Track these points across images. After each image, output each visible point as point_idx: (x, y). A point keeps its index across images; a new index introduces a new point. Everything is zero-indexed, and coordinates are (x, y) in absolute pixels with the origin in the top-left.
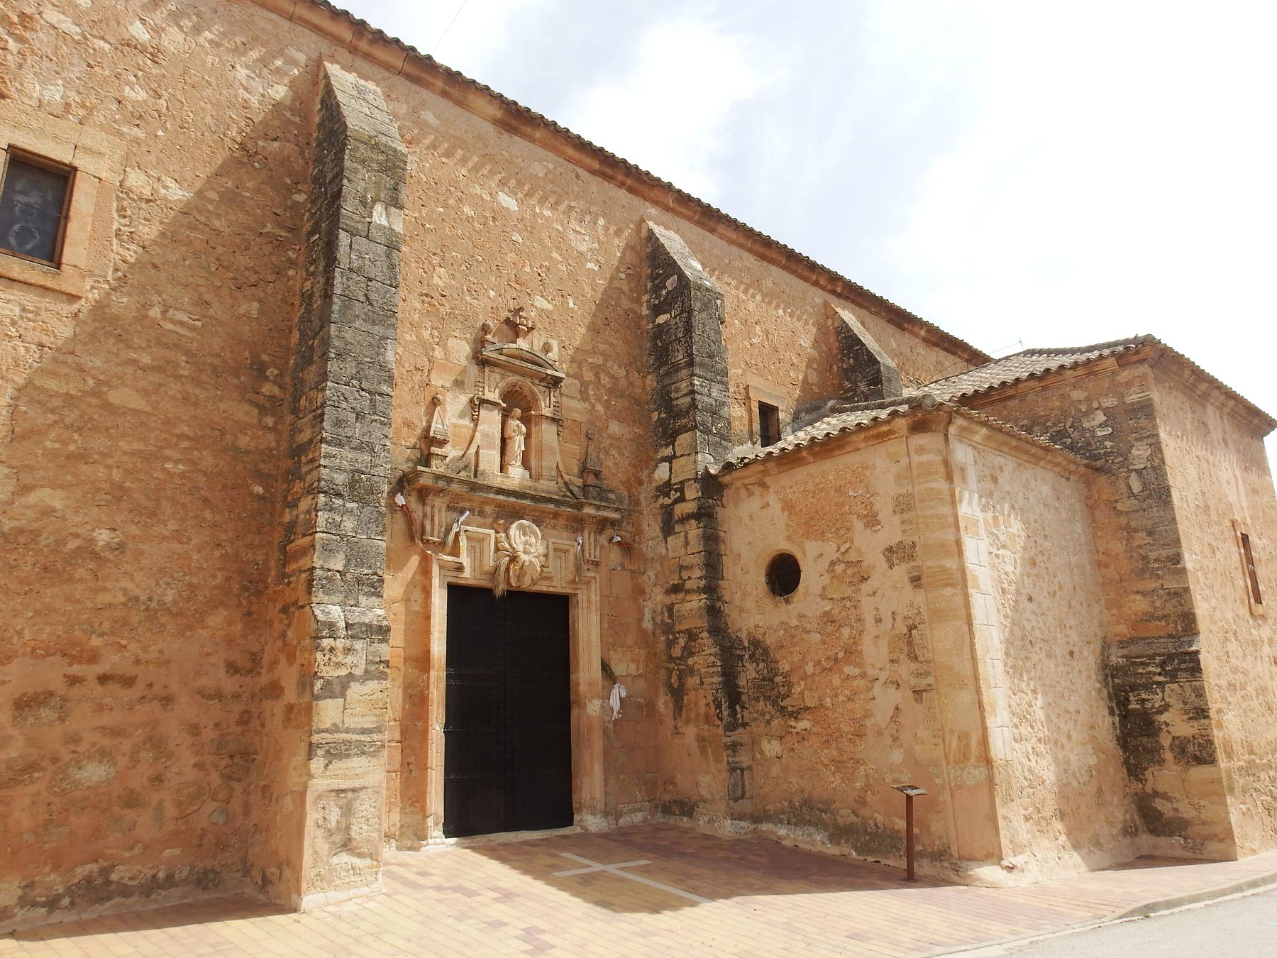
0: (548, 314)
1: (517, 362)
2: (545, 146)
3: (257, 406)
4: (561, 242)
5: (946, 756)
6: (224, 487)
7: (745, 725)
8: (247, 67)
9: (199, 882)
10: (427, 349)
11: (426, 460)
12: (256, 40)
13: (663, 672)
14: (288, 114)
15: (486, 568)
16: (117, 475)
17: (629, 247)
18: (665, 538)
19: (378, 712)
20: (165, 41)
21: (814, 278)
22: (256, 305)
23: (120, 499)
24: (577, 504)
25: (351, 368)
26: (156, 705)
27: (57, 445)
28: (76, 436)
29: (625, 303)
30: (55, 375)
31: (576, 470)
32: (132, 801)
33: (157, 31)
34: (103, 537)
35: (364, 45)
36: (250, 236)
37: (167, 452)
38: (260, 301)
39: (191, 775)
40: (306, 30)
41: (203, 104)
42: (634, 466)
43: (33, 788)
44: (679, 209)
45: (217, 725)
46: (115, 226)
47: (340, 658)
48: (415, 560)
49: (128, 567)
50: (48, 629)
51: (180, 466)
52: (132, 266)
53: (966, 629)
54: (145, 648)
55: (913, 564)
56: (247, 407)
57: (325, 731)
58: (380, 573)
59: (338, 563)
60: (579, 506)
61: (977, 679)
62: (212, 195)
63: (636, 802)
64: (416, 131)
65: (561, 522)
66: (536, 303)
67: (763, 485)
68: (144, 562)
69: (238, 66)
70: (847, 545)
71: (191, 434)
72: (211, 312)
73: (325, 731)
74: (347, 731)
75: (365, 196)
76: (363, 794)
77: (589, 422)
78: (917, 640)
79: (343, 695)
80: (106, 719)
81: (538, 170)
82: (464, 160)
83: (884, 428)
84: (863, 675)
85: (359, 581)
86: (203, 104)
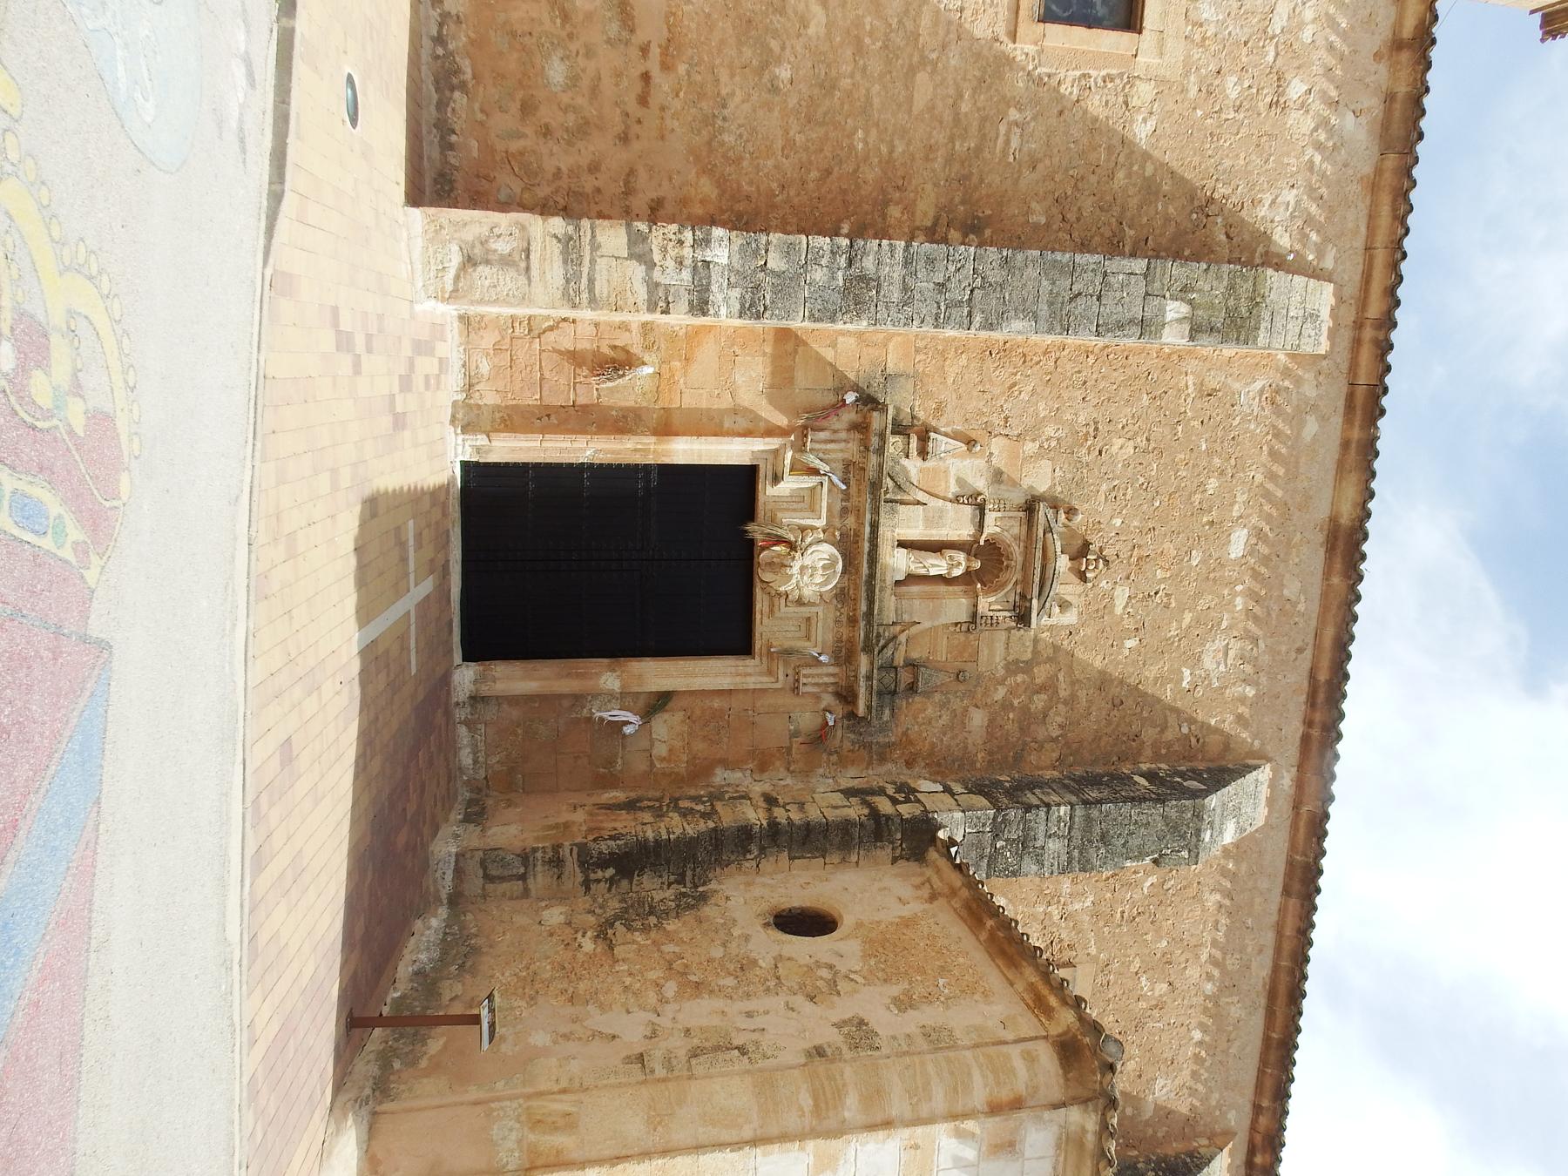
0: (1109, 608)
1: (1039, 554)
2: (1325, 595)
3: (935, 224)
4: (1207, 626)
5: (540, 1094)
6: (844, 192)
7: (587, 884)
8: (1298, 203)
9: (442, 175)
10: (1032, 431)
11: (900, 429)
12: (1331, 211)
13: (658, 794)
14: (1260, 249)
15: (780, 515)
16: (846, 83)
17: (1227, 743)
18: (841, 791)
19: (612, 299)
20: (1294, 116)
21: (1265, 1103)
22: (1043, 220)
23: (822, 86)
24: (875, 679)
25: (995, 276)
26: (619, 128)
27: (868, 27)
28: (879, 44)
29: (1149, 734)
30: (936, 23)
31: (915, 655)
32: (527, 108)
33: (1303, 106)
34: (784, 73)
35: (1368, 333)
36: (1116, 211)
37: (874, 132)
38: (1048, 225)
39: (549, 165)
40: (1361, 267)
41: (1242, 156)
42: (931, 754)
43: (546, 18)
44: (1302, 824)
45: (598, 190)
46: (1093, 73)
47: (672, 253)
48: (782, 420)
49: (755, 98)
50: (693, 25)
51: (860, 146)
52: (1056, 90)
53: (747, 1133)
54: (675, 116)
55: (845, 1049)
56: (931, 213)
57: (593, 236)
58: (767, 315)
59: (775, 262)
60: (868, 648)
61: (666, 1152)
62: (1149, 170)
63: (487, 755)
64: (1289, 410)
65: (845, 632)
66: (1119, 590)
67: (933, 897)
68: (761, 113)
69: (1294, 191)
70: (860, 980)
71: (895, 155)
72: (1026, 172)
73: (593, 236)
74: (593, 262)
75: (1193, 290)
76: (523, 280)
77: (979, 677)
78: (721, 1056)
79: (631, 256)
80: (607, 83)
81: (1291, 589)
82: (1272, 476)
83: (1053, 1001)
84: (663, 1000)
85: (757, 288)
86: (1242, 156)
